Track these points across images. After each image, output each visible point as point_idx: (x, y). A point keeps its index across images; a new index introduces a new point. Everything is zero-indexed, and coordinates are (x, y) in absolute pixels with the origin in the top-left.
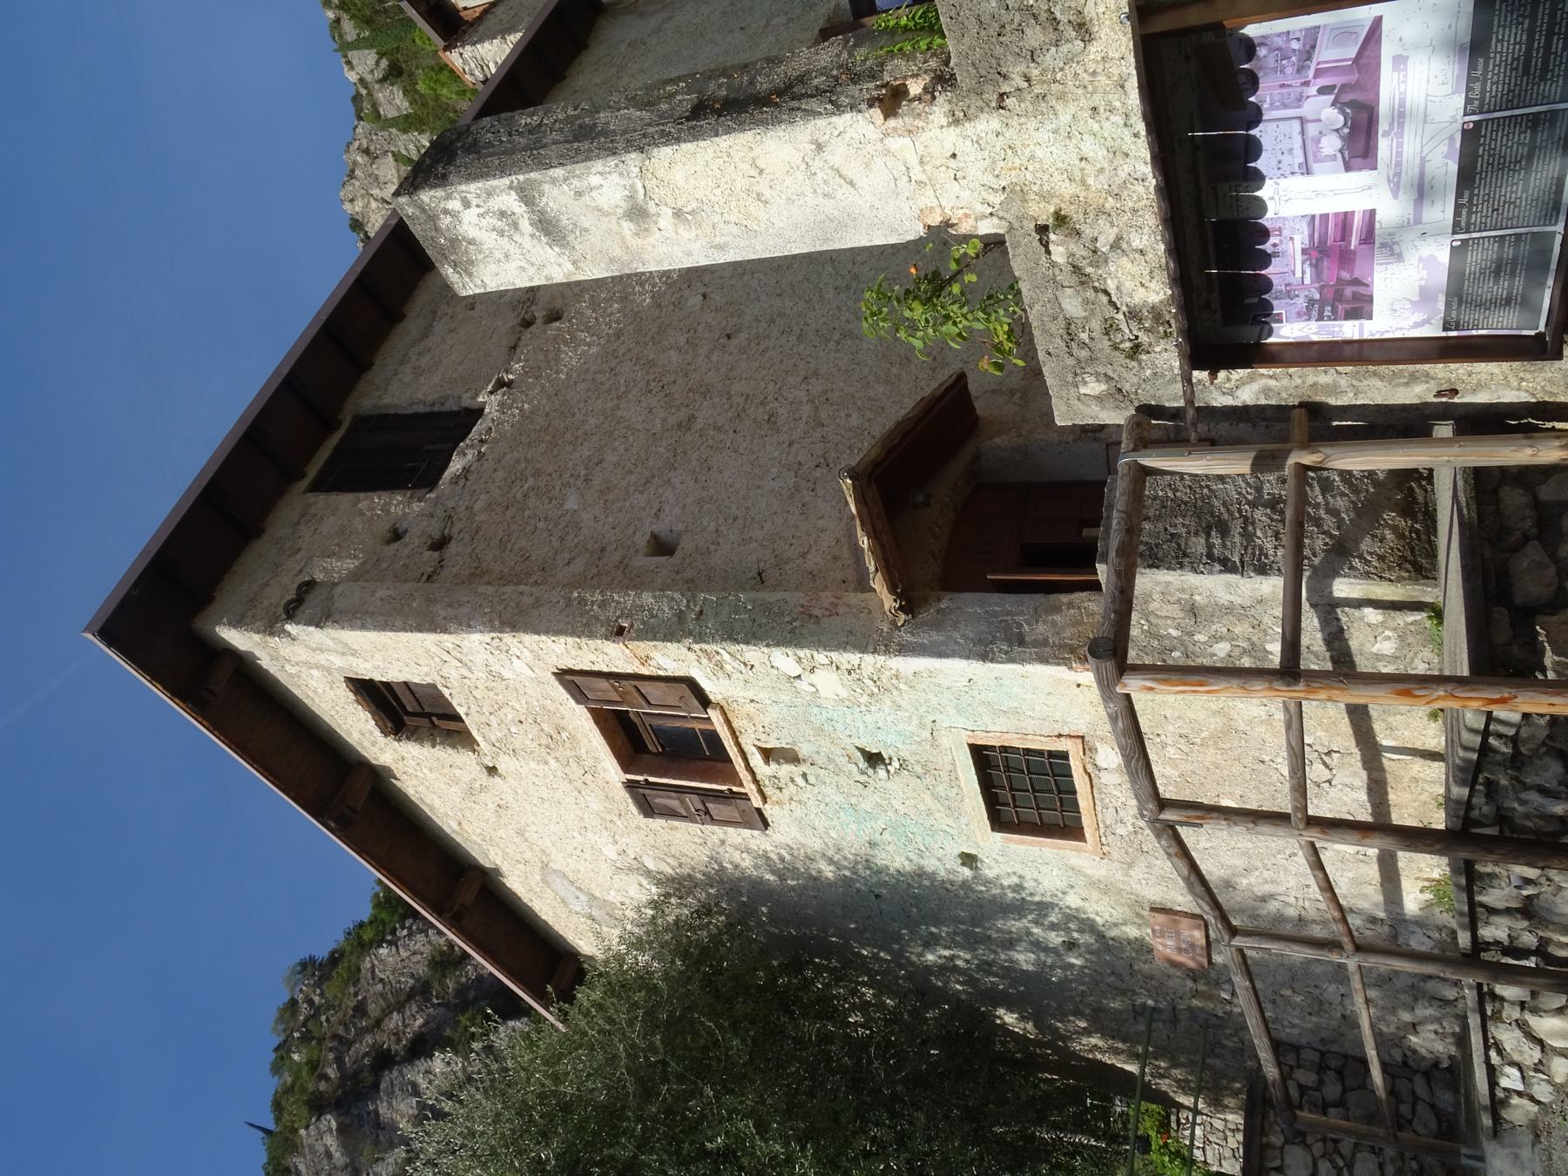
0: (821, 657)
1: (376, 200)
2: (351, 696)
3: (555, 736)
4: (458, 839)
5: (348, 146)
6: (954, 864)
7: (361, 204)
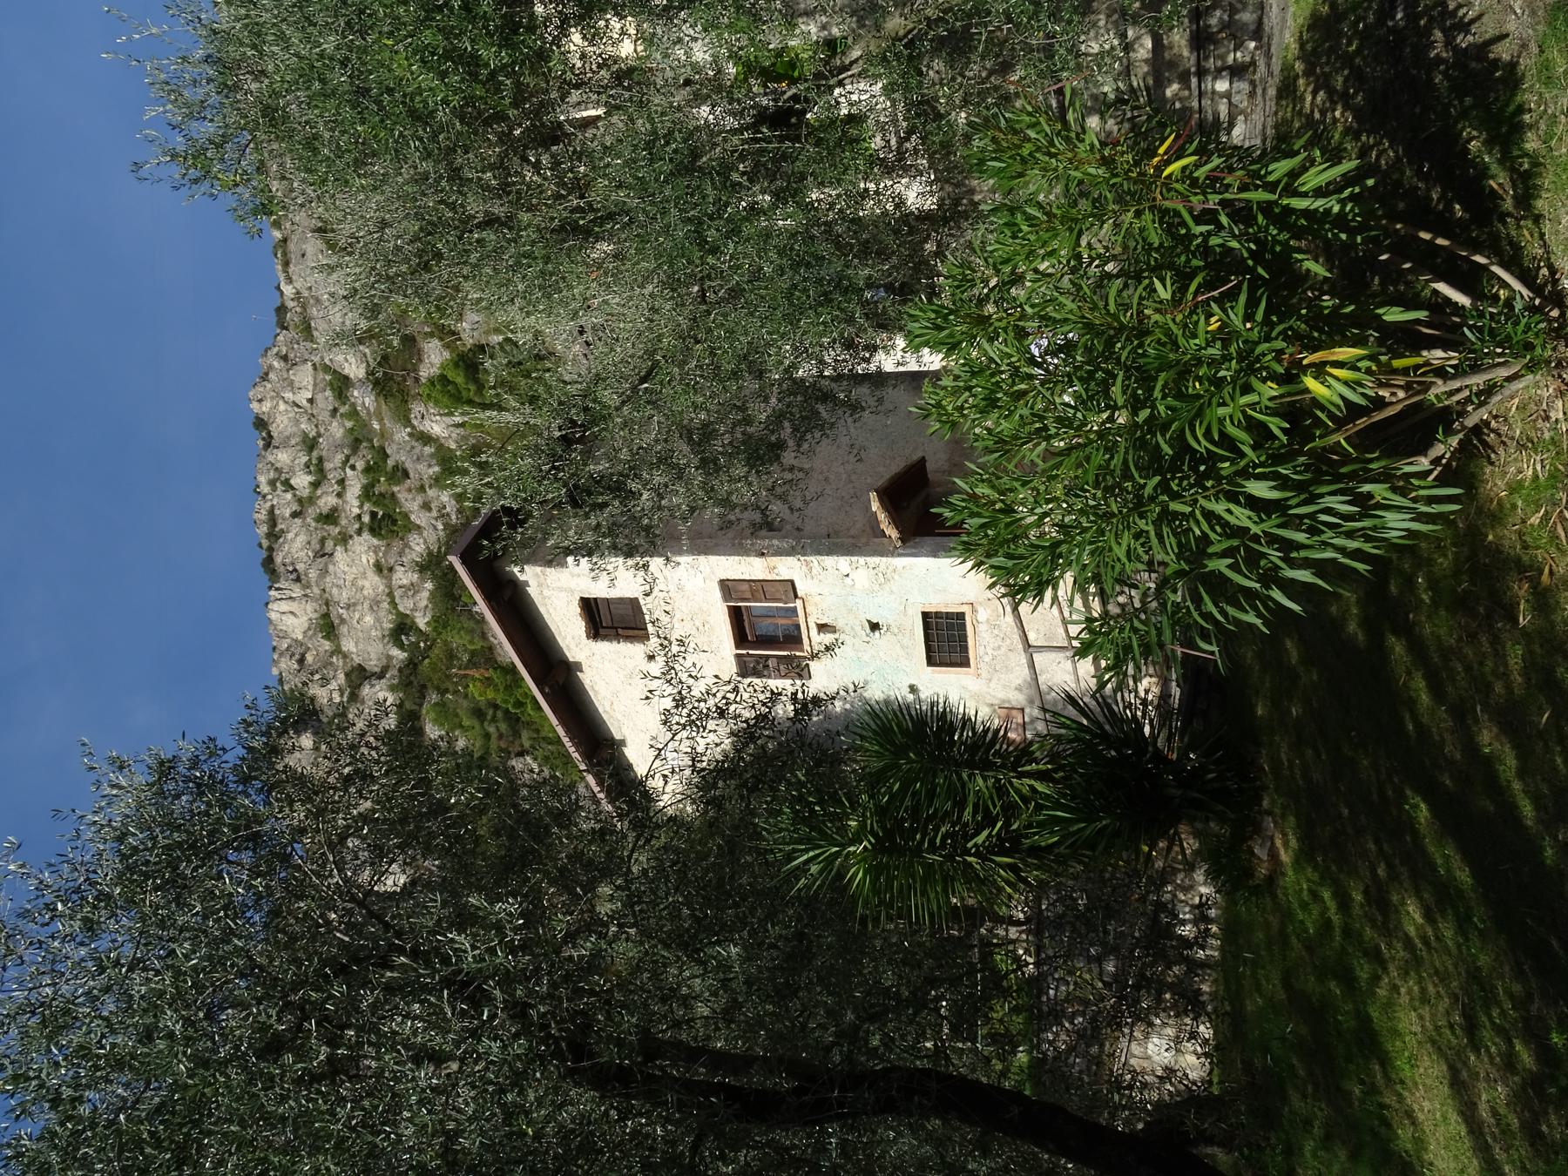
0: (862, 560)
1: (286, 402)
2: (579, 610)
3: (701, 628)
4: (605, 717)
5: (266, 351)
6: (905, 691)
7: (269, 405)
